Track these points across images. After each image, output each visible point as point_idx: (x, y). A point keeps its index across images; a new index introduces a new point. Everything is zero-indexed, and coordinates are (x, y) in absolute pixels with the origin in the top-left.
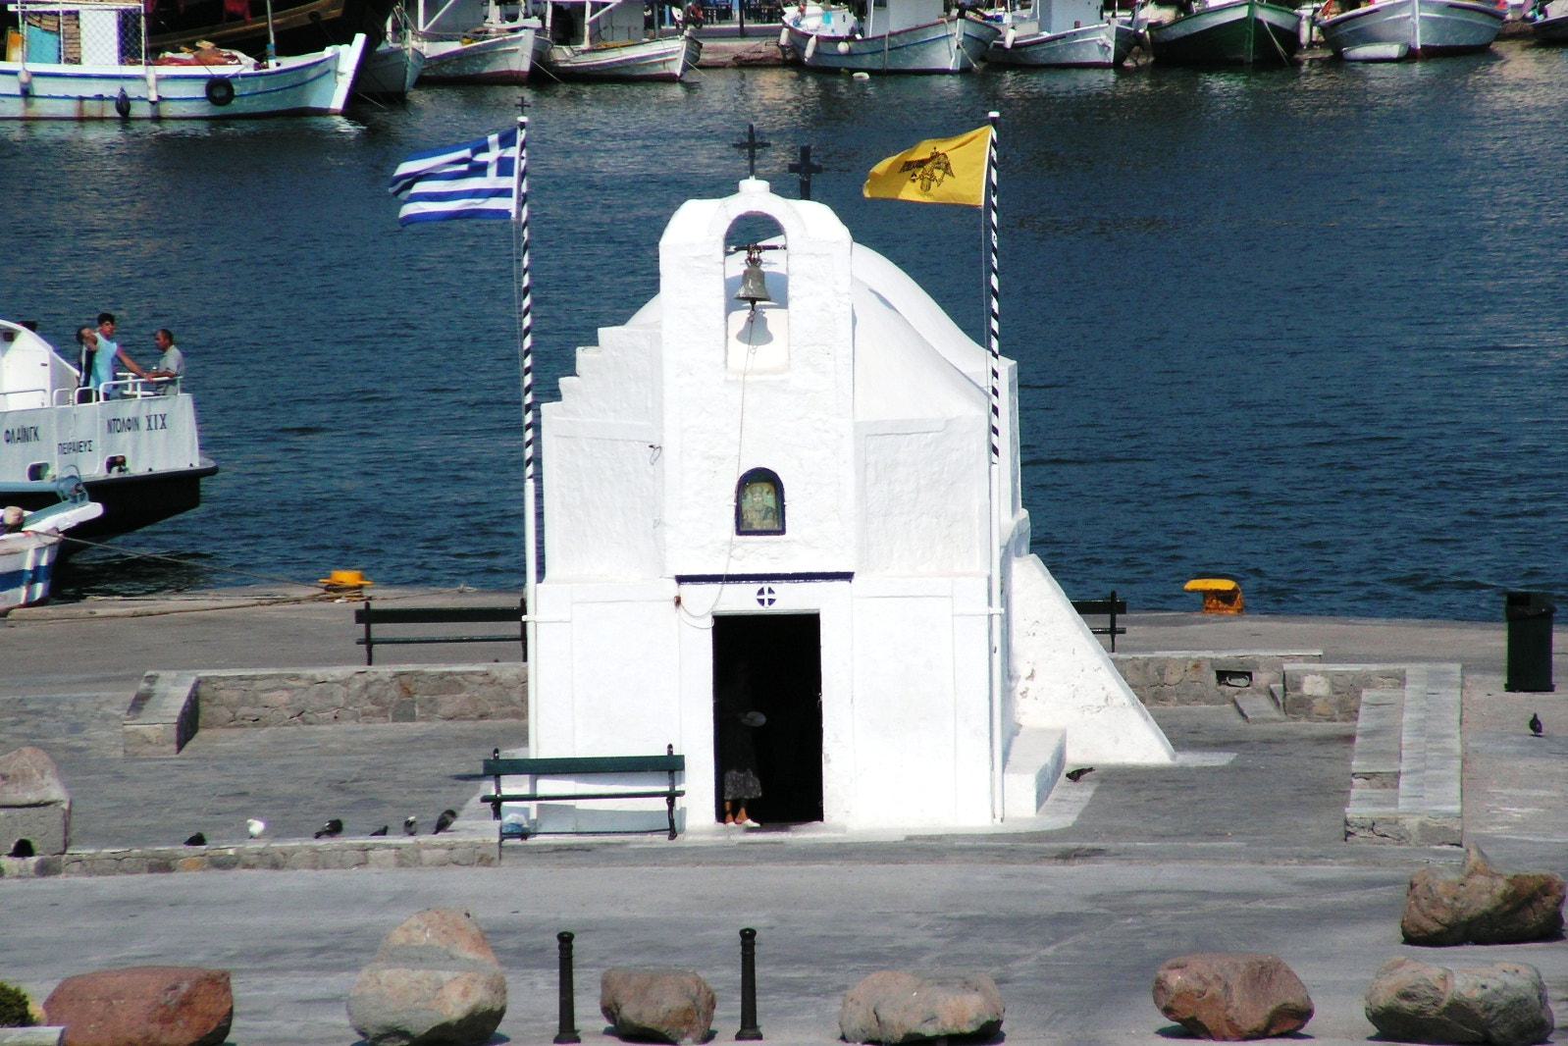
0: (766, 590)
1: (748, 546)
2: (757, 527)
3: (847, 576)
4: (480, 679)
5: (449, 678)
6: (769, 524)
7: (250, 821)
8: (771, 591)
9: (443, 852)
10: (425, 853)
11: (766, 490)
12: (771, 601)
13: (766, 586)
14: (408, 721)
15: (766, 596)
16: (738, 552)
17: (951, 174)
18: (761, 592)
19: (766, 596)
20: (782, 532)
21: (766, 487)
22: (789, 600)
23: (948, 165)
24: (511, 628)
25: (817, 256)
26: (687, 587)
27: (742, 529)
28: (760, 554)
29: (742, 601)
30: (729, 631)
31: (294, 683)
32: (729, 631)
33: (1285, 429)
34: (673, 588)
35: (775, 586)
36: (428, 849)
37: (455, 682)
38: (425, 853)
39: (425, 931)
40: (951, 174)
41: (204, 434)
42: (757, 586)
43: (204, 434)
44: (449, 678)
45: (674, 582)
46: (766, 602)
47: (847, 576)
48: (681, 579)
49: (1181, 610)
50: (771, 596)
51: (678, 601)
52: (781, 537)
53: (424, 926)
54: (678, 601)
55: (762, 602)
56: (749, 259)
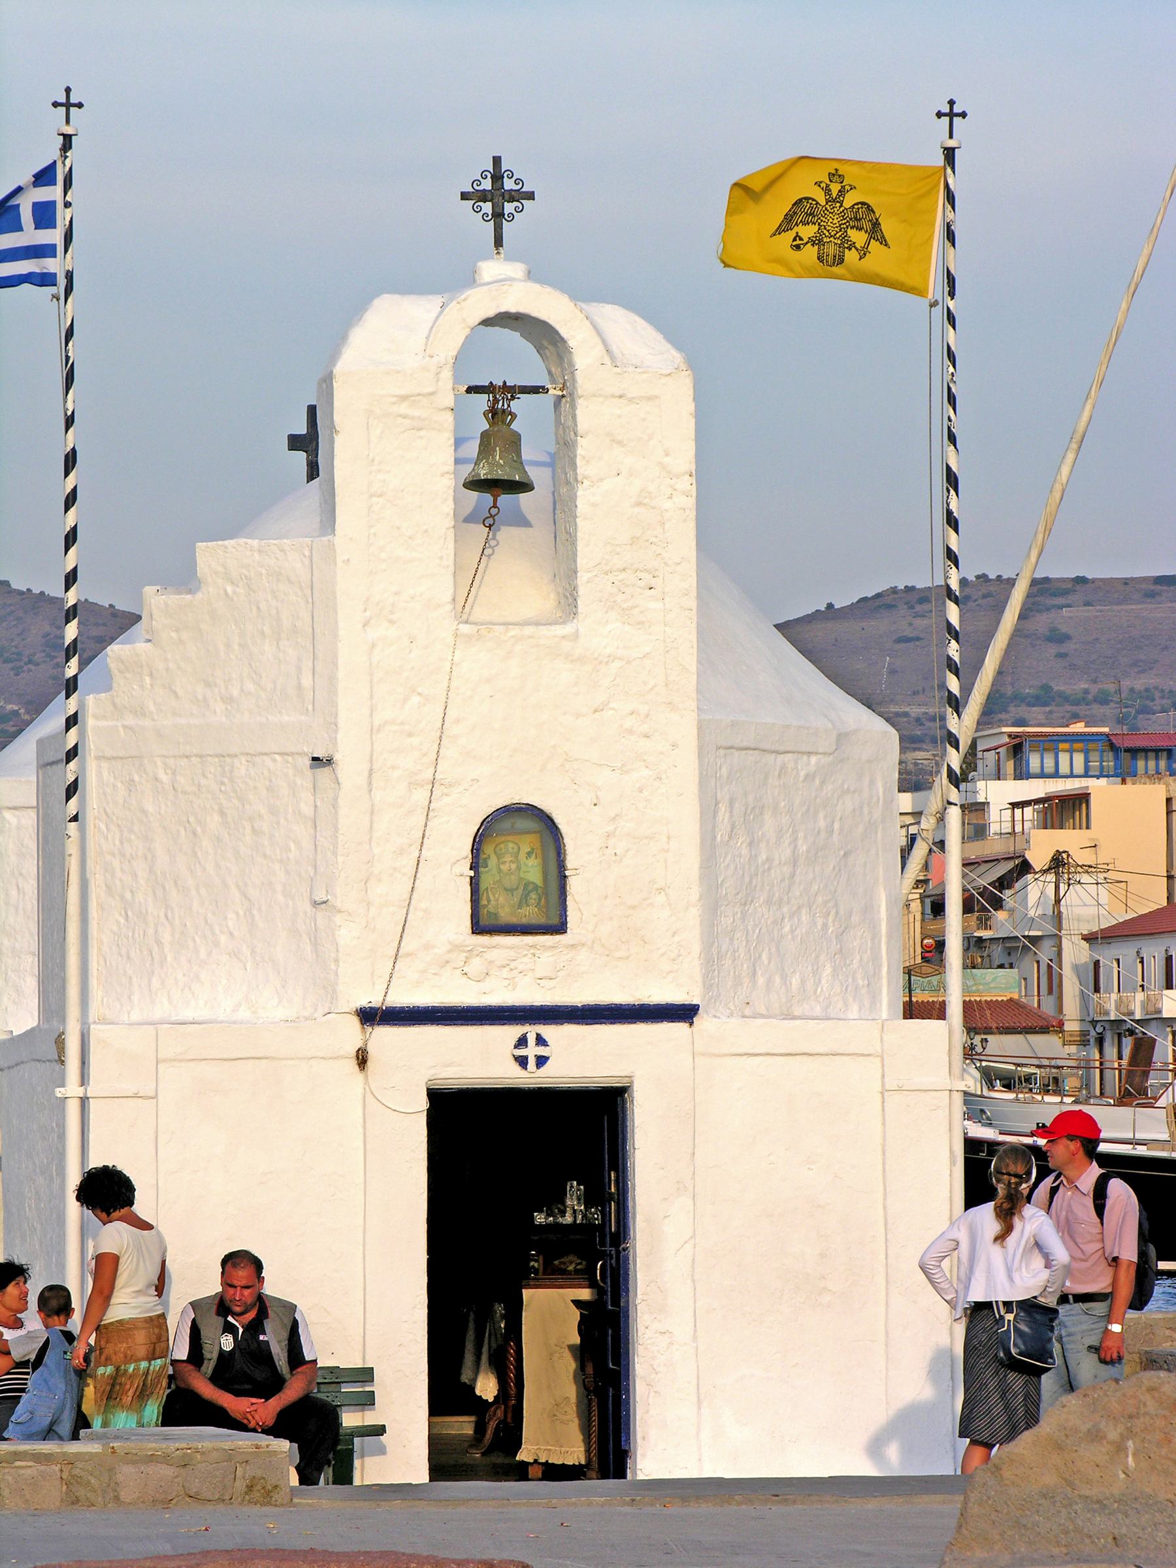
1: (493, 955)
2: (506, 916)
3: (685, 1013)
6: (530, 914)
8: (541, 1041)
9: (167, 1471)
10: (126, 1473)
11: (525, 849)
12: (541, 1061)
13: (532, 1031)
14: (1099, 964)
15: (531, 1051)
16: (476, 966)
17: (884, 242)
18: (522, 1042)
19: (531, 1051)
20: (560, 928)
23: (876, 224)
24: (965, 862)
25: (631, 400)
26: (385, 1036)
27: (485, 921)
34: (352, 1034)
35: (547, 1031)
36: (134, 1463)
38: (126, 1473)
39: (1119, 1448)
40: (884, 242)
42: (512, 1032)
45: (355, 1021)
47: (685, 1013)
48: (369, 1016)
50: (542, 1051)
51: (362, 1059)
52: (558, 937)
53: (1113, 1434)
54: (362, 1059)
55: (522, 1062)
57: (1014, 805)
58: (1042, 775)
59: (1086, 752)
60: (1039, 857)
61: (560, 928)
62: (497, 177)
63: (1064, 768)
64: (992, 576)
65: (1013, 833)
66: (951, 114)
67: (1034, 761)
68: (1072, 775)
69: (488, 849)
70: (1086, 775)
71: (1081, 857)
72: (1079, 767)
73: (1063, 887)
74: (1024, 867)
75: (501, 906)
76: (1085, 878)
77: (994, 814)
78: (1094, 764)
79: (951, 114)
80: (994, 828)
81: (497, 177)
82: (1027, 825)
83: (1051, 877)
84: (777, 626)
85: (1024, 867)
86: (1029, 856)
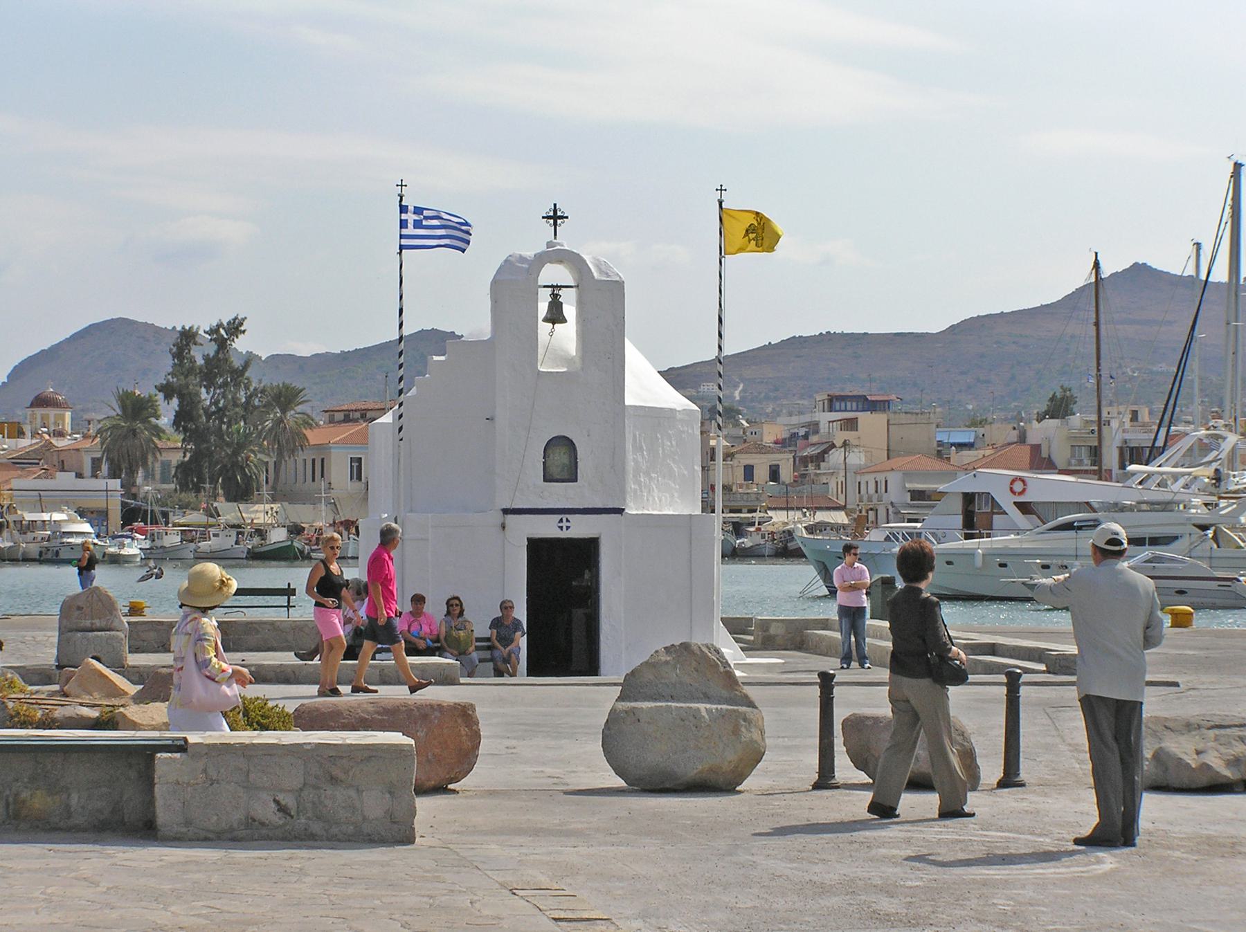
0: (564, 520)
4: (268, 627)
5: (250, 626)
7: (194, 700)
8: (568, 521)
12: (568, 528)
13: (564, 517)
18: (561, 521)
19: (564, 524)
21: (563, 450)
22: (579, 528)
26: (511, 518)
28: (560, 494)
29: (548, 528)
30: (538, 549)
31: (160, 627)
32: (538, 549)
33: (10, 670)
35: (569, 517)
37: (255, 629)
41: (849, 428)
43: (849, 428)
44: (250, 626)
45: (501, 512)
46: (564, 528)
48: (506, 511)
49: (1165, 673)
50: (568, 524)
55: (561, 528)
56: (553, 294)
57: (829, 422)
58: (840, 411)
59: (858, 402)
60: (838, 443)
61: (575, 480)
62: (555, 211)
63: (849, 408)
64: (824, 333)
65: (829, 433)
66: (555, 217)
67: (837, 405)
68: (852, 411)
69: (550, 451)
70: (856, 411)
71: (854, 442)
72: (854, 407)
73: (847, 453)
74: (833, 446)
75: (555, 471)
76: (855, 450)
77: (821, 426)
78: (860, 406)
79: (555, 217)
80: (822, 431)
81: (555, 211)
82: (835, 430)
83: (843, 449)
84: (659, 372)
85: (833, 446)
86: (835, 442)
